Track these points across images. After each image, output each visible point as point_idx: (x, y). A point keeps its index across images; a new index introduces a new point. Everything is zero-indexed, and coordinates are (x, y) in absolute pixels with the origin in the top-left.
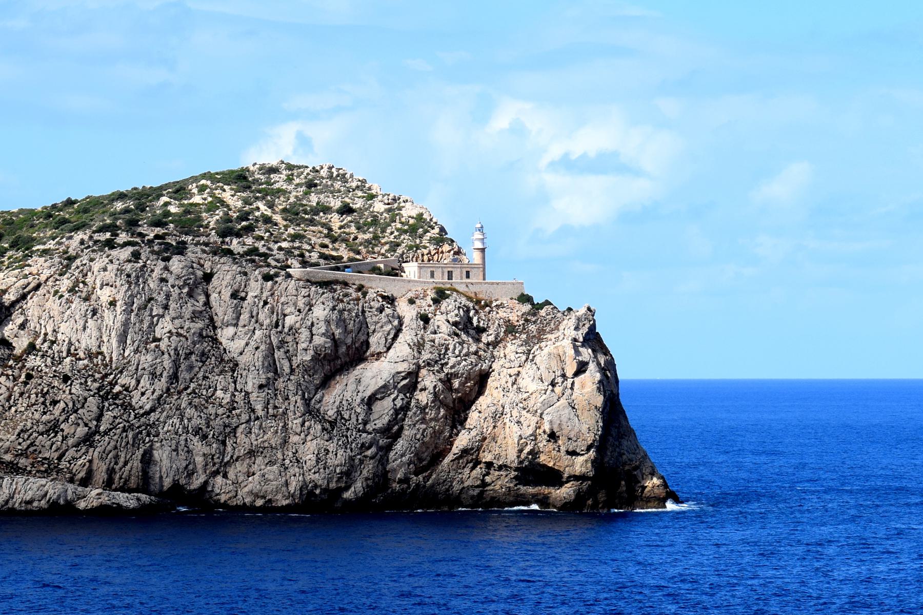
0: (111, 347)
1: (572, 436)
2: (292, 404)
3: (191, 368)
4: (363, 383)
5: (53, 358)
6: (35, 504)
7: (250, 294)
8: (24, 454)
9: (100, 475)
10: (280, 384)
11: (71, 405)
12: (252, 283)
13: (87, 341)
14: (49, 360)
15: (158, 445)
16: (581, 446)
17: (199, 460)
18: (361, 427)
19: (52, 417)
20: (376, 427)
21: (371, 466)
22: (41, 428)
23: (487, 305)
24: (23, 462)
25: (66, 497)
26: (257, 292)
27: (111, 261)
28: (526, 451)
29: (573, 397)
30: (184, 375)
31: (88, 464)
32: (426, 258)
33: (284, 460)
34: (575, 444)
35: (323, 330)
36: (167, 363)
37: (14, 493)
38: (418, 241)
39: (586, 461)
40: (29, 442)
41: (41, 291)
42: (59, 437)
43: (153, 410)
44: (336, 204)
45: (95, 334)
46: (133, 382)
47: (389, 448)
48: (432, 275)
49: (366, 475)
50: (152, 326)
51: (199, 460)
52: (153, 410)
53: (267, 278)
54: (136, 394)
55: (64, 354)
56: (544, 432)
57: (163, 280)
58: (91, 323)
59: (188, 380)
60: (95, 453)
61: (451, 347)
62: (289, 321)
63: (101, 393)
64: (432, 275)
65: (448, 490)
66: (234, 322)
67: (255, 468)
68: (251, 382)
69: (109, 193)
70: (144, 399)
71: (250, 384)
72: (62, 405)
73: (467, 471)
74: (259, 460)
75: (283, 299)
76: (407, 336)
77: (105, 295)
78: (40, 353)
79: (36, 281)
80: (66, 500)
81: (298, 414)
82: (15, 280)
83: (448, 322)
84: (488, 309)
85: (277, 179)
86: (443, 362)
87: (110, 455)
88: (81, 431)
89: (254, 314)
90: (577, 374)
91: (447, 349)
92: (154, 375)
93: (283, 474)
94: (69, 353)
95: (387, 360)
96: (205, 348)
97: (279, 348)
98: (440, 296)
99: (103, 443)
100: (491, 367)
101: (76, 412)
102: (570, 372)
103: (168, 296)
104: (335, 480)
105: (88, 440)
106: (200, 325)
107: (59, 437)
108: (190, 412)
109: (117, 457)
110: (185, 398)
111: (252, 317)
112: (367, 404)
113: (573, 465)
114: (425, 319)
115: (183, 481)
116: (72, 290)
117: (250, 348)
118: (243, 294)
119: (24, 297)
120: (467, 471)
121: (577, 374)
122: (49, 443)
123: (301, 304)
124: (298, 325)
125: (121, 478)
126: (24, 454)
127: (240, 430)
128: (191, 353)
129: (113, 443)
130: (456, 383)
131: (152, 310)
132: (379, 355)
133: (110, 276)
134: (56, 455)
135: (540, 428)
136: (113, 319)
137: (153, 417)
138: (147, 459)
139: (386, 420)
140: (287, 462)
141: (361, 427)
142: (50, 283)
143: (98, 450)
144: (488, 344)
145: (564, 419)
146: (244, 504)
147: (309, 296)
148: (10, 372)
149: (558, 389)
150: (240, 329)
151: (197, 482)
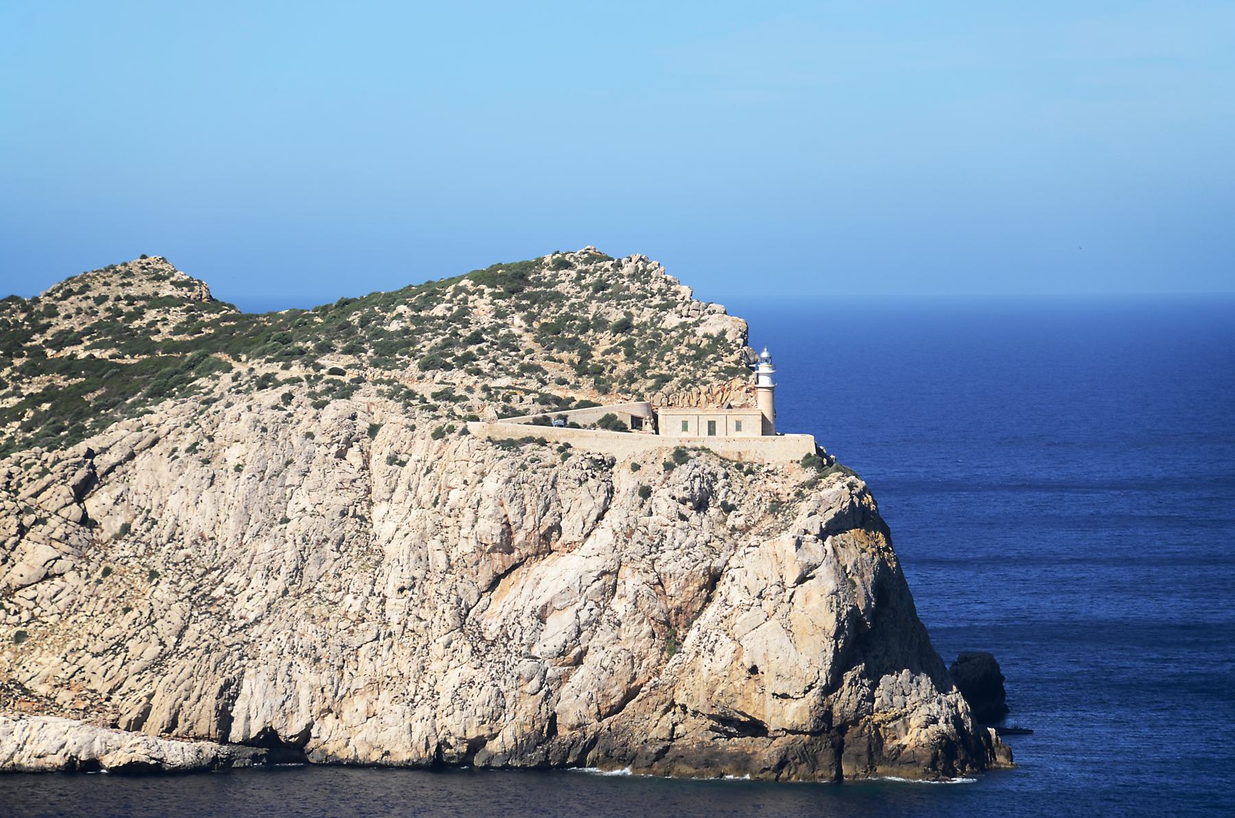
0: (228, 532)
1: (783, 672)
2: (439, 613)
3: (322, 561)
4: (542, 586)
5: (148, 545)
6: (49, 759)
7: (415, 457)
8: (66, 685)
9: (159, 717)
10: (430, 588)
11: (146, 614)
12: (419, 443)
13: (197, 522)
14: (143, 547)
15: (252, 671)
16: (795, 688)
17: (304, 695)
18: (524, 649)
19: (118, 631)
20: (545, 650)
21: (530, 706)
22: (99, 646)
23: (750, 472)
24: (64, 696)
25: (91, 747)
26: (423, 454)
27: (250, 408)
28: (719, 691)
29: (791, 616)
30: (311, 571)
31: (144, 700)
32: (703, 397)
33: (416, 694)
34: (787, 684)
35: (489, 511)
36: (290, 553)
37: (25, 743)
38: (699, 374)
39: (802, 709)
40: (76, 667)
41: (156, 449)
42: (119, 660)
43: (257, 621)
44: (616, 315)
45: (210, 512)
46: (243, 581)
47: (562, 679)
48: (685, 427)
49: (522, 719)
50: (284, 500)
51: (304, 695)
52: (257, 621)
53: (438, 434)
54: (242, 598)
55: (164, 540)
56: (742, 665)
57: (310, 435)
58: (206, 496)
59: (314, 579)
60: (160, 684)
61: (669, 535)
62: (454, 496)
63: (194, 597)
64: (685, 427)
65: (625, 744)
66: (387, 496)
67: (377, 706)
68: (391, 580)
69: (518, 261)
70: (249, 606)
71: (390, 585)
72: (134, 614)
73: (656, 715)
74: (385, 695)
75: (451, 466)
76: (614, 518)
77: (233, 455)
78: (133, 539)
79: (153, 436)
80: (90, 753)
81: (443, 630)
82: (124, 432)
83: (674, 498)
84: (750, 477)
85: (563, 278)
86: (653, 556)
87: (182, 687)
88: (153, 650)
89: (413, 486)
90: (802, 580)
91: (664, 537)
92: (270, 572)
93: (408, 716)
94: (171, 539)
95: (581, 553)
96: (353, 531)
97: (434, 535)
98: (676, 460)
99: (178, 668)
100: (727, 563)
101: (152, 624)
102: (790, 580)
103: (310, 458)
104: (475, 725)
105: (158, 664)
106: (347, 498)
107: (119, 660)
108: (305, 625)
109: (190, 689)
110: (301, 606)
111: (410, 489)
112: (538, 617)
113: (781, 714)
114: (646, 492)
115: (276, 725)
116: (192, 449)
117: (400, 534)
118: (403, 458)
119: (132, 456)
120: (656, 715)
121: (802, 580)
122: (103, 669)
123: (470, 476)
124: (461, 504)
125: (186, 720)
126: (66, 685)
127: (362, 651)
128: (326, 540)
129: (188, 670)
130: (671, 588)
131: (285, 477)
132: (571, 547)
133: (243, 427)
134: (109, 686)
135: (737, 659)
136: (235, 489)
137: (256, 631)
138: (229, 692)
139: (559, 641)
140: (418, 698)
141: (524, 649)
142: (171, 437)
143: (166, 679)
144: (734, 529)
145: (773, 647)
146: (356, 757)
147: (483, 461)
148: (84, 566)
149: (768, 605)
150: (394, 506)
151: (293, 728)
